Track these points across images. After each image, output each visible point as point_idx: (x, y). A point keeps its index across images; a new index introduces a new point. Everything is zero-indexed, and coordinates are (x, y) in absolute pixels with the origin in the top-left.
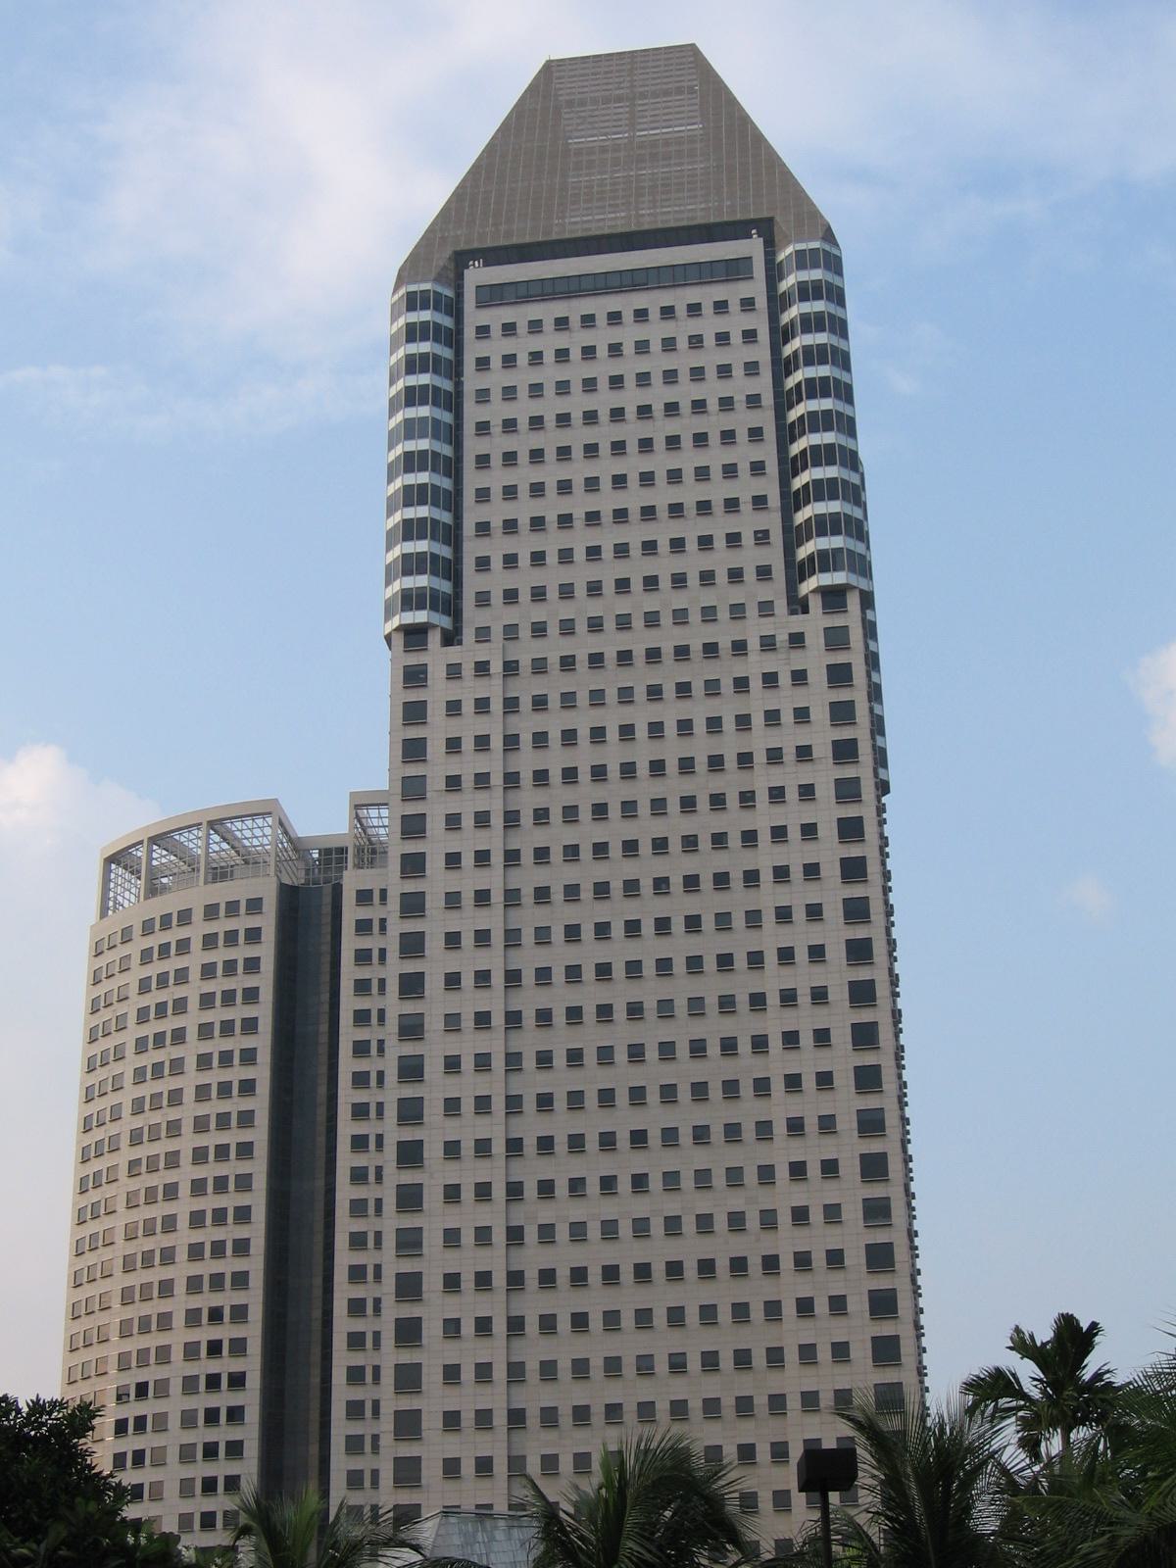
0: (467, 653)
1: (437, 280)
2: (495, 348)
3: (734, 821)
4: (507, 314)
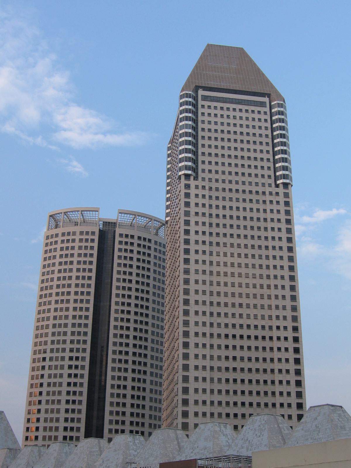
0: (200, 183)
1: (192, 91)
2: (206, 111)
3: (263, 234)
4: (209, 103)
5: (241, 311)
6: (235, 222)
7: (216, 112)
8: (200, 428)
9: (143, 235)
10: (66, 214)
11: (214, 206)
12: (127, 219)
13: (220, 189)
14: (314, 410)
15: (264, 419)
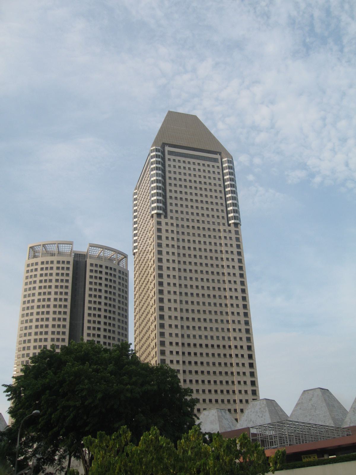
4: (174, 157)
5: (205, 325)
6: (198, 253)
7: (180, 164)
8: (204, 414)
9: (109, 265)
10: (44, 246)
11: (181, 240)
12: (96, 252)
13: (185, 226)
14: (308, 393)
15: (263, 404)
